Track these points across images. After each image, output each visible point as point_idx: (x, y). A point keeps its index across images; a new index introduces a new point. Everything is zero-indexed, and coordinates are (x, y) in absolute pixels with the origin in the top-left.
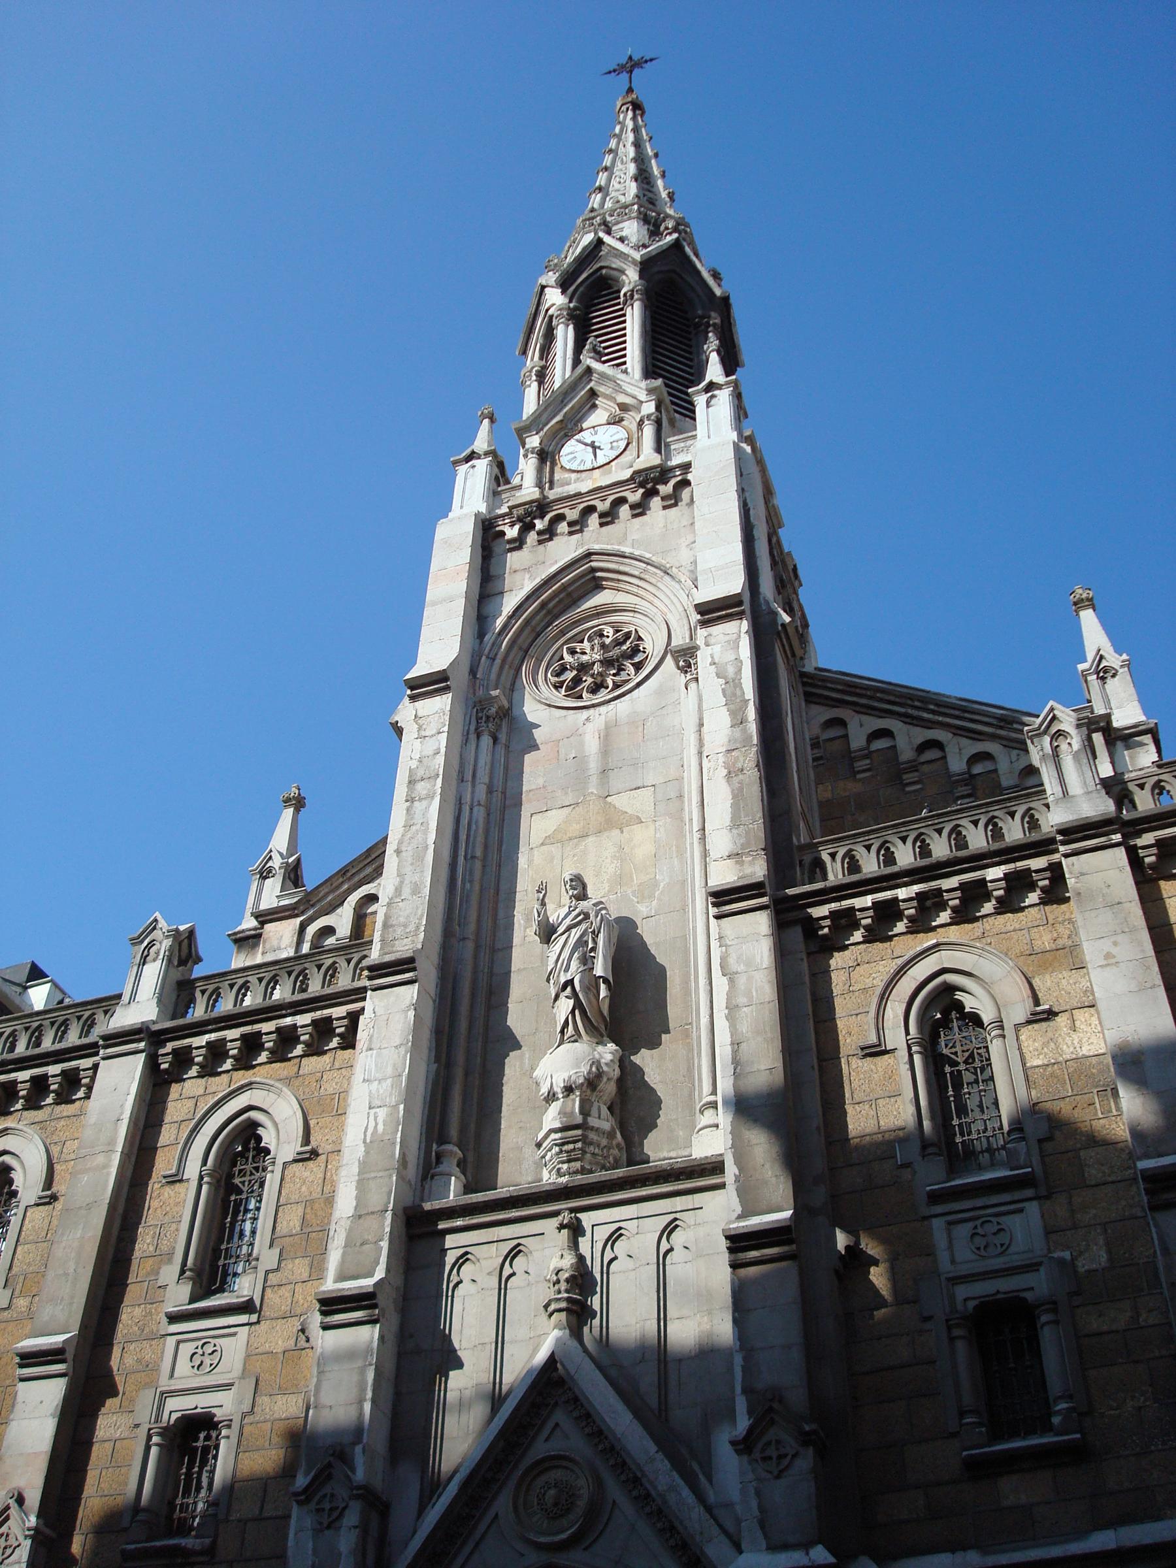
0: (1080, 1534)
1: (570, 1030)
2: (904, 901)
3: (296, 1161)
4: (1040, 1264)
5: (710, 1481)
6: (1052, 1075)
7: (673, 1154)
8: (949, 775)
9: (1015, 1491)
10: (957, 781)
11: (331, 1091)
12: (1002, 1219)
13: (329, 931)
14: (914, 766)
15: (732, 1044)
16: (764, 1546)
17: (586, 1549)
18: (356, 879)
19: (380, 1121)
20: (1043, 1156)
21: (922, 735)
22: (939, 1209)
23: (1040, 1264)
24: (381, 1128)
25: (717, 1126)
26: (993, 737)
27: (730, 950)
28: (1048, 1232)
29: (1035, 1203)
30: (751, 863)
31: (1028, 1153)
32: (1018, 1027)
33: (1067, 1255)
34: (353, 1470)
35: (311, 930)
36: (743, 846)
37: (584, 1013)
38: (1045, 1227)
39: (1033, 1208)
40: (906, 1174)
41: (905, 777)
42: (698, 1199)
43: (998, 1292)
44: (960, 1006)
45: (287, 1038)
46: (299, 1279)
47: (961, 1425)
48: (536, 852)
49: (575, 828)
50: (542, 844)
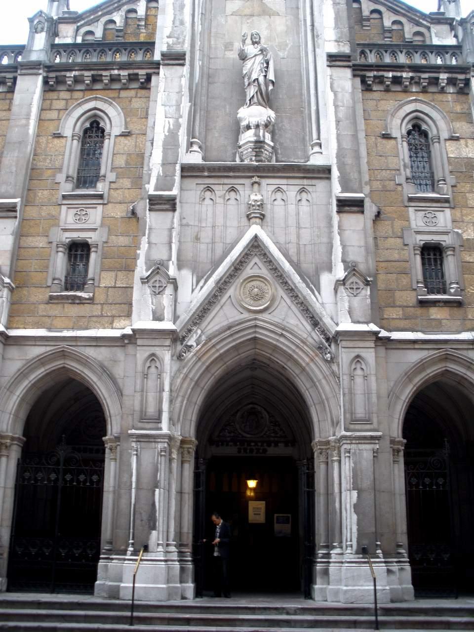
0: (459, 332)
1: (255, 100)
2: (405, 78)
3: (120, 135)
4: (449, 232)
5: (319, 293)
6: (458, 162)
7: (296, 160)
8: (383, 26)
9: (435, 313)
10: (387, 30)
11: (136, 107)
12: (87, 210)
13: (91, 33)
14: (368, 20)
15: (336, 121)
16: (350, 321)
17: (270, 314)
18: (105, 11)
19: (171, 124)
20: (453, 192)
21: (374, 6)
22: (65, 202)
23: (96, 229)
24: (172, 127)
25: (321, 153)
26: (404, 15)
27: (335, 82)
28: (454, 221)
29: (102, 206)
30: (343, 46)
31: (447, 190)
32: (446, 140)
33: (460, 231)
34: (168, 270)
35: (83, 30)
36: (340, 38)
37: (261, 94)
38: (452, 219)
39: (448, 211)
40: (399, 188)
41: (364, 22)
42: (314, 182)
43: (79, 237)
44: (98, 123)
45: (397, 81)
46: (126, 187)
47: (53, 283)
48: (229, 18)
49: (247, 11)
50: (232, 15)
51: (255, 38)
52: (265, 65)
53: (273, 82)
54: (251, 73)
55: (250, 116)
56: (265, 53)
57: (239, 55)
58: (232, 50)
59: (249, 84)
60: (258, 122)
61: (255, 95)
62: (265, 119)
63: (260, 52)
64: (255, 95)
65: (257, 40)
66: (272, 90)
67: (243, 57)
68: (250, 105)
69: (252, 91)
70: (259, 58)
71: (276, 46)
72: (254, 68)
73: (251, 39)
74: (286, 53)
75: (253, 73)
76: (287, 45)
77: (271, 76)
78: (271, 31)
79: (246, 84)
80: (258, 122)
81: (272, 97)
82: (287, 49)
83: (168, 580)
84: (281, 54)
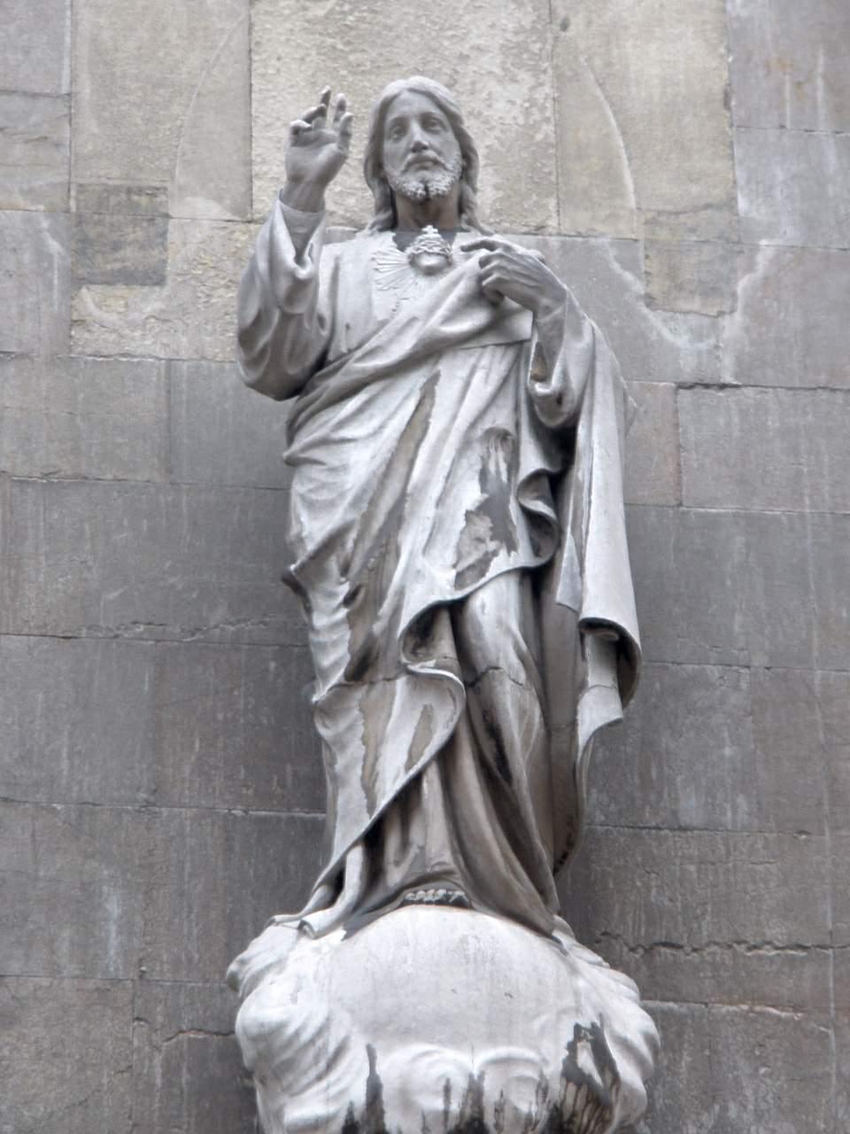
1: (431, 836)
37: (496, 775)
51: (421, 160)
52: (532, 460)
53: (618, 649)
54: (386, 546)
55: (387, 1027)
56: (524, 324)
57: (246, 337)
58: (155, 278)
59: (362, 668)
60: (475, 1091)
61: (431, 789)
62: (554, 1068)
63: (476, 319)
64: (431, 789)
65: (441, 182)
66: (606, 733)
67: (296, 364)
68: (378, 898)
69: (391, 741)
70: (471, 387)
71: (624, 243)
72: (410, 478)
73: (376, 168)
74: (733, 326)
75: (411, 539)
76: (737, 243)
77: (601, 585)
78: (560, 79)
79: (335, 656)
80: (475, 1091)
81: (595, 804)
82: (742, 285)
83: (630, 504)
84: (679, 339)
